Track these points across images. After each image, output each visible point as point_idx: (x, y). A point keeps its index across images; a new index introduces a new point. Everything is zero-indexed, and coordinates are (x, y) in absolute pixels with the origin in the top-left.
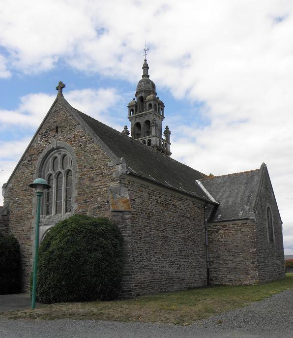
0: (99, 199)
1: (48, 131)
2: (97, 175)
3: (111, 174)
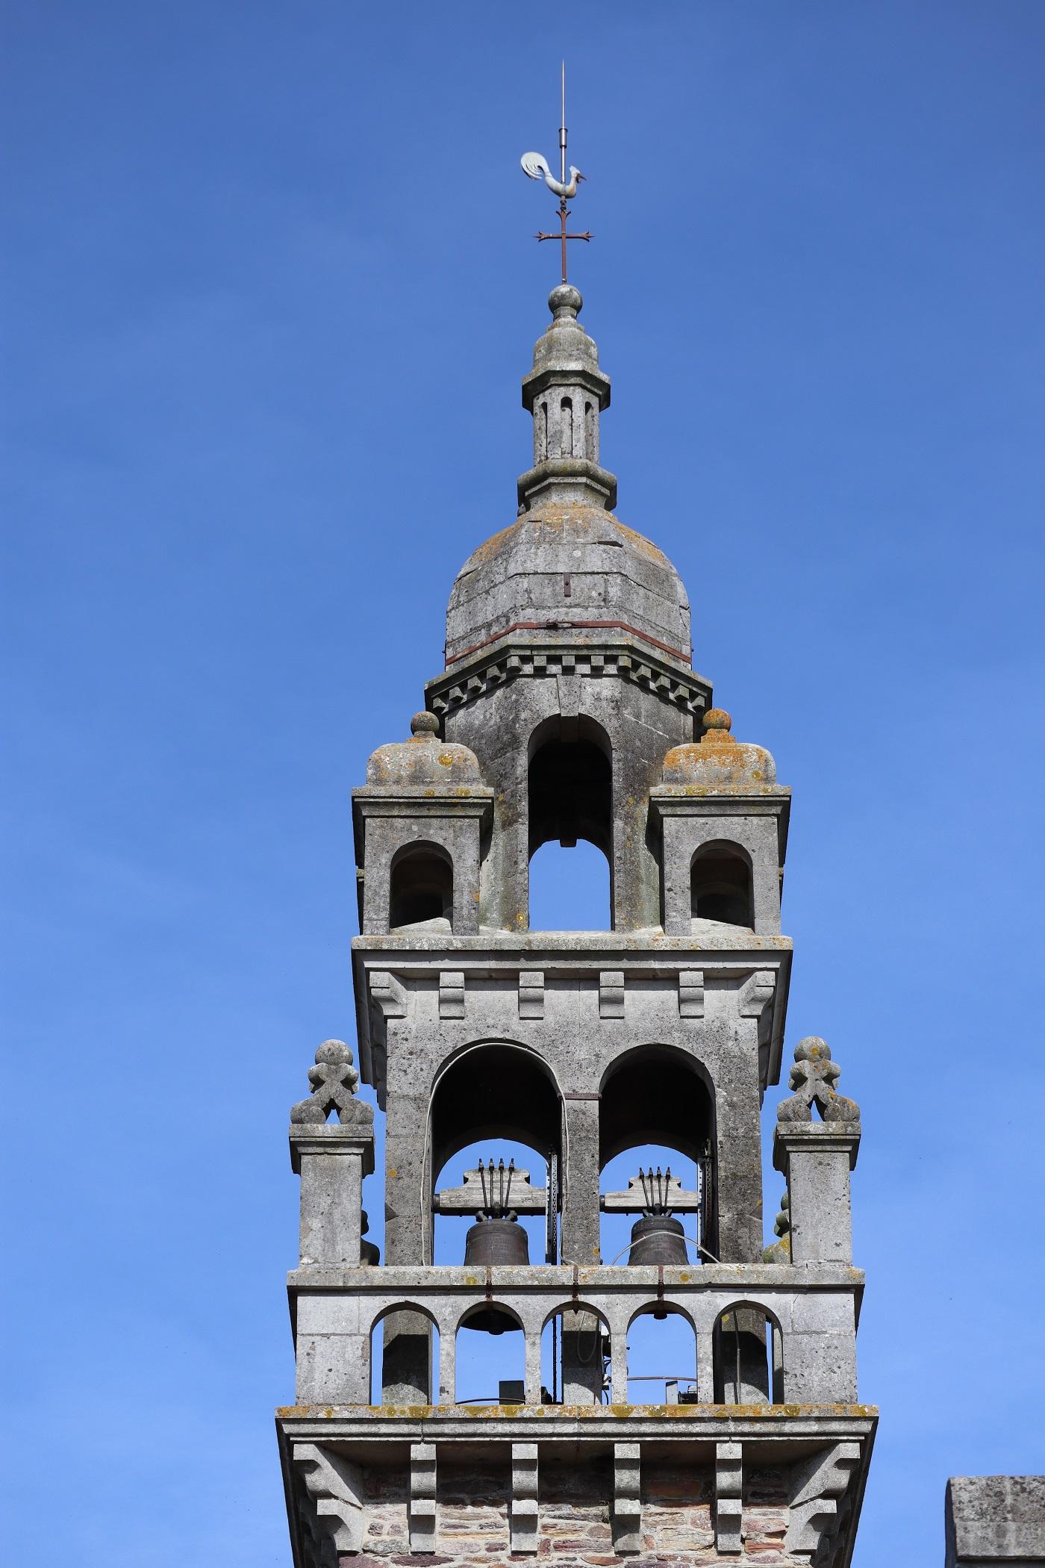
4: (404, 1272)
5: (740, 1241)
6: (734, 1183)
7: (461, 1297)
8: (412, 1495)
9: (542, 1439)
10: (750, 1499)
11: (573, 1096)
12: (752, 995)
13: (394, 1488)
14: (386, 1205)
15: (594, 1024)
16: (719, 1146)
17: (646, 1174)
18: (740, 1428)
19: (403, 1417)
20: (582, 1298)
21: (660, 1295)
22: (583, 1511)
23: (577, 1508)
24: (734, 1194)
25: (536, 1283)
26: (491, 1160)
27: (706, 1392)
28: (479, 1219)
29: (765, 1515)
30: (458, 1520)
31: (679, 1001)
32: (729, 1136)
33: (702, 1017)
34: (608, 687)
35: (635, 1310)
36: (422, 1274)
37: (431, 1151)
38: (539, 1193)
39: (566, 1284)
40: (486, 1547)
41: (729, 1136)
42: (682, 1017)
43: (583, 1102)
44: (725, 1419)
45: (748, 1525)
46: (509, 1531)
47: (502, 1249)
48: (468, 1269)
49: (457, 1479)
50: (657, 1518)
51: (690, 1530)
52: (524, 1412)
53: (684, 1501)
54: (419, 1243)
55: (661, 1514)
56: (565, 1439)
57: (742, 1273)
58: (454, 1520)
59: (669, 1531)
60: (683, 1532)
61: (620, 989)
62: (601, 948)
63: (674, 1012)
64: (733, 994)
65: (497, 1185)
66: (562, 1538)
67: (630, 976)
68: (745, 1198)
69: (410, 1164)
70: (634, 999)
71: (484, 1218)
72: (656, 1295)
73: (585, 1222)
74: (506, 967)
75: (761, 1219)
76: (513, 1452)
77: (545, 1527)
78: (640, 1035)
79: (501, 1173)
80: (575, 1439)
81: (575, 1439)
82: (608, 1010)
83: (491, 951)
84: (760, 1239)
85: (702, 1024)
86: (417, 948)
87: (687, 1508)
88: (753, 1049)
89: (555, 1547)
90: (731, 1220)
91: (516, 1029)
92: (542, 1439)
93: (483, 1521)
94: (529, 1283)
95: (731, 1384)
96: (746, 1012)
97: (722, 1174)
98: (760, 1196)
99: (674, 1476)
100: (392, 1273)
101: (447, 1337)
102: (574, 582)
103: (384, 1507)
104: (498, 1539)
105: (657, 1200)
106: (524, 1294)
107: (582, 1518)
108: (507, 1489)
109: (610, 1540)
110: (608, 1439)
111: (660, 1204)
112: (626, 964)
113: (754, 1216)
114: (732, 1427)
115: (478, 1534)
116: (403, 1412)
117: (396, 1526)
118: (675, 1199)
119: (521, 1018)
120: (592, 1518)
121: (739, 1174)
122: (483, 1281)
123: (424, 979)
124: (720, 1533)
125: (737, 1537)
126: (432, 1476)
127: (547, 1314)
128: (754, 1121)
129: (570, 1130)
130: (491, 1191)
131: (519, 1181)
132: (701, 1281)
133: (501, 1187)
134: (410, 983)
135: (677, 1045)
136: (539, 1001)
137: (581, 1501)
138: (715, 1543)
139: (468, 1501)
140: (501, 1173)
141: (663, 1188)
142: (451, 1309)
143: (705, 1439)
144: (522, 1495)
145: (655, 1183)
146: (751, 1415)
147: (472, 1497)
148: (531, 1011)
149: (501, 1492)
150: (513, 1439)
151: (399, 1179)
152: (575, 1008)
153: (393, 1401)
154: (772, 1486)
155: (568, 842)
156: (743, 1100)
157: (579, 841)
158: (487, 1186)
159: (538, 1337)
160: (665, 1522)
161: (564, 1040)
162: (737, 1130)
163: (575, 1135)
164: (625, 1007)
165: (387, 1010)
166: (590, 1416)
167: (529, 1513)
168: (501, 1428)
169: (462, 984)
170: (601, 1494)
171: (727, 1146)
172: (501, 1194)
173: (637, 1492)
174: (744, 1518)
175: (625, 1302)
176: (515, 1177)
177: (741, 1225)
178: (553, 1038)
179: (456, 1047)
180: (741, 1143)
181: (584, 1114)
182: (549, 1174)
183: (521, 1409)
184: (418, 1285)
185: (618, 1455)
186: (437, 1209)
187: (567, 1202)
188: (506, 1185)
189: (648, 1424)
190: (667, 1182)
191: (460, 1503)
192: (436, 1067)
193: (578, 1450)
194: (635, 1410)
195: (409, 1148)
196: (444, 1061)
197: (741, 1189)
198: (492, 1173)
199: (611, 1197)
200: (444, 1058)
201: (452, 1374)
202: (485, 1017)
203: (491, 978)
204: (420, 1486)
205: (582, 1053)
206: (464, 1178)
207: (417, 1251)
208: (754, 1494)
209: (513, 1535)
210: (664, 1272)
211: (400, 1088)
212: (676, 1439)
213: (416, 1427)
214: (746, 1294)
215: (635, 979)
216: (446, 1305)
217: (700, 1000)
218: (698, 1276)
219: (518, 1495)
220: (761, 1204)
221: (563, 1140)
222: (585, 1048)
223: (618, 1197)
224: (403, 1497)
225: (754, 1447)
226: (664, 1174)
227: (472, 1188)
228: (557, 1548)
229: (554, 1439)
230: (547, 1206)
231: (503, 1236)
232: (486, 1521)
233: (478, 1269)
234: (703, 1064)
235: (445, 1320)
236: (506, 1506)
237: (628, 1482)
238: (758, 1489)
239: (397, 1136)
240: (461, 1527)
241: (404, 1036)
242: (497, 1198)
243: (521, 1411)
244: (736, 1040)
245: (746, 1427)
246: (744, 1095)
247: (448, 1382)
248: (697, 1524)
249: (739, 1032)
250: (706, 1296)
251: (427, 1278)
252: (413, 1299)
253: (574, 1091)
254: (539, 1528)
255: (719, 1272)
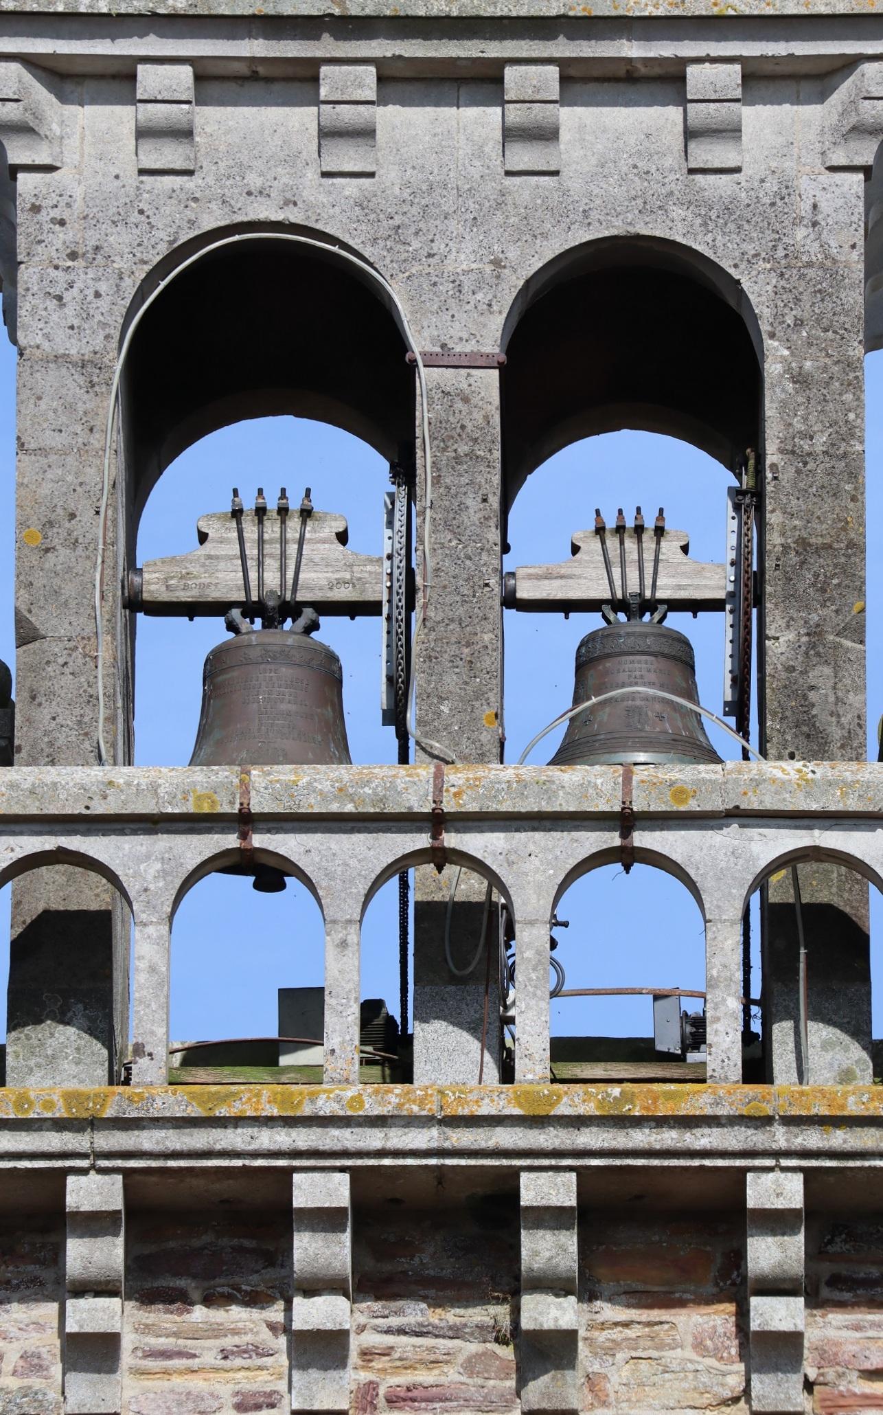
4: (55, 784)
5: (812, 695)
6: (803, 563)
7: (183, 837)
8: (68, 1286)
9: (359, 1162)
10: (825, 1292)
11: (443, 359)
12: (853, 120)
13: (31, 1268)
14: (17, 612)
15: (490, 189)
16: (769, 475)
17: (611, 523)
18: (799, 1140)
19: (49, 1115)
20: (451, 840)
21: (626, 834)
22: (452, 1316)
23: (439, 1311)
24: (801, 586)
25: (349, 808)
26: (260, 491)
27: (724, 1056)
28: (232, 627)
29: (857, 1328)
30: (172, 1340)
31: (685, 132)
32: (793, 452)
33: (737, 170)
35: (569, 867)
36: (94, 788)
37: (122, 485)
38: (369, 568)
39: (415, 810)
40: (235, 1400)
41: (793, 452)
42: (692, 171)
43: (464, 372)
44: (767, 1121)
45: (820, 1351)
46: (286, 1363)
47: (282, 701)
48: (201, 776)
49: (172, 1244)
50: (617, 1334)
51: (691, 1361)
52: (320, 1102)
53: (677, 1295)
54: (92, 699)
55: (626, 1325)
56: (410, 1162)
57: (808, 786)
58: (162, 1340)
59: (644, 1365)
60: (674, 1366)
61: (552, 106)
62: (505, 12)
63: (672, 160)
64: (811, 113)
65: (273, 549)
66: (404, 1379)
67: (572, 72)
68: (827, 596)
69: (72, 516)
70: (582, 128)
71: (244, 624)
72: (617, 834)
73: (466, 651)
74: (290, 55)
75: (862, 642)
76: (295, 1192)
77: (367, 1355)
78: (594, 215)
79: (283, 522)
80: (433, 1162)
81: (433, 1162)
82: (523, 156)
83: (254, 16)
84: (860, 688)
85: (736, 187)
86: (83, 9)
87: (684, 1311)
88: (853, 246)
89: (389, 1401)
90: (794, 647)
91: (312, 198)
92: (359, 1162)
93: (229, 1342)
94: (335, 808)
95: (788, 1025)
96: (839, 159)
97: (774, 539)
98: (861, 591)
99: (656, 1238)
100: (27, 786)
101: (151, 930)
103: (7, 1311)
104: (261, 1382)
105: (633, 587)
106: (323, 832)
107: (450, 1333)
108: (282, 1266)
109: (511, 1383)
110: (505, 1162)
111: (641, 595)
112: (563, 48)
113: (846, 637)
114: (780, 1137)
115: (217, 1370)
116: (49, 1105)
117: (32, 1355)
118: (674, 581)
119: (325, 175)
120: (472, 1334)
121: (813, 540)
122: (232, 803)
123: (100, 77)
124: (759, 1371)
125: (796, 1380)
126: (114, 1245)
127: (374, 876)
128: (851, 416)
129: (433, 438)
130: (260, 564)
131: (324, 541)
132: (716, 803)
133: (283, 555)
134: (68, 87)
135: (679, 239)
136: (366, 133)
137: (449, 1293)
138: (747, 1392)
139: (196, 1295)
140: (283, 522)
141: (649, 556)
142: (158, 866)
143: (720, 1163)
144: (312, 1288)
145: (630, 544)
146: (824, 1111)
147: (206, 1284)
148: (347, 157)
149: (271, 1273)
150: (297, 1163)
151: (47, 550)
152: (447, 150)
153: (32, 1063)
154: (874, 1263)
156: (825, 368)
158: (252, 551)
159: (353, 929)
160: (634, 1343)
161: (422, 225)
162: (811, 438)
163: (444, 450)
164: (562, 147)
165: (17, 153)
166: (466, 1112)
167: (329, 1326)
168: (268, 1139)
169: (189, 95)
170: (492, 1278)
171: (787, 475)
172: (283, 570)
173: (570, 1280)
174: (812, 1336)
175: (546, 850)
176: (314, 531)
177: (815, 660)
178: (398, 220)
179: (175, 241)
180: (819, 468)
181: (466, 400)
182: (390, 524)
183: (313, 1098)
184: (85, 812)
185: (528, 1197)
186: (135, 604)
187: (425, 607)
188: (292, 549)
189: (595, 1129)
190: (658, 543)
191: (177, 1298)
192: (130, 287)
193: (440, 1183)
194: (565, 1099)
195: (70, 478)
196: (150, 274)
197: (816, 576)
198: (261, 522)
199: (530, 577)
200: (148, 268)
201: (162, 1014)
202: (243, 168)
203: (254, 77)
204: (85, 1268)
205: (463, 257)
206: (199, 531)
207: (86, 719)
208: (835, 1281)
209: (296, 1375)
210: (634, 783)
211: (47, 337)
212: (656, 1162)
213: (79, 1136)
214: (816, 832)
215: (586, 80)
216: (148, 857)
217: (732, 132)
218: (712, 792)
219: (305, 1286)
220: (863, 610)
221: (419, 462)
222: (468, 246)
223: (546, 578)
224: (50, 1287)
225: (832, 1179)
226: (650, 523)
227: (217, 557)
229: (387, 1162)
230: (385, 598)
231: (285, 671)
232: (236, 1340)
233: (224, 774)
234: (738, 282)
235: (146, 890)
236: (280, 1305)
237: (550, 1258)
238: (843, 1269)
239: (42, 451)
240: (180, 1354)
241: (55, 213)
242: (272, 579)
243: (313, 1102)
244: (815, 224)
245: (812, 1139)
246: (828, 355)
247: (152, 1033)
248: (706, 1349)
249: (823, 205)
250: (730, 836)
251: (105, 798)
252: (75, 843)
253: (443, 346)
254: (354, 1357)
255: (757, 783)
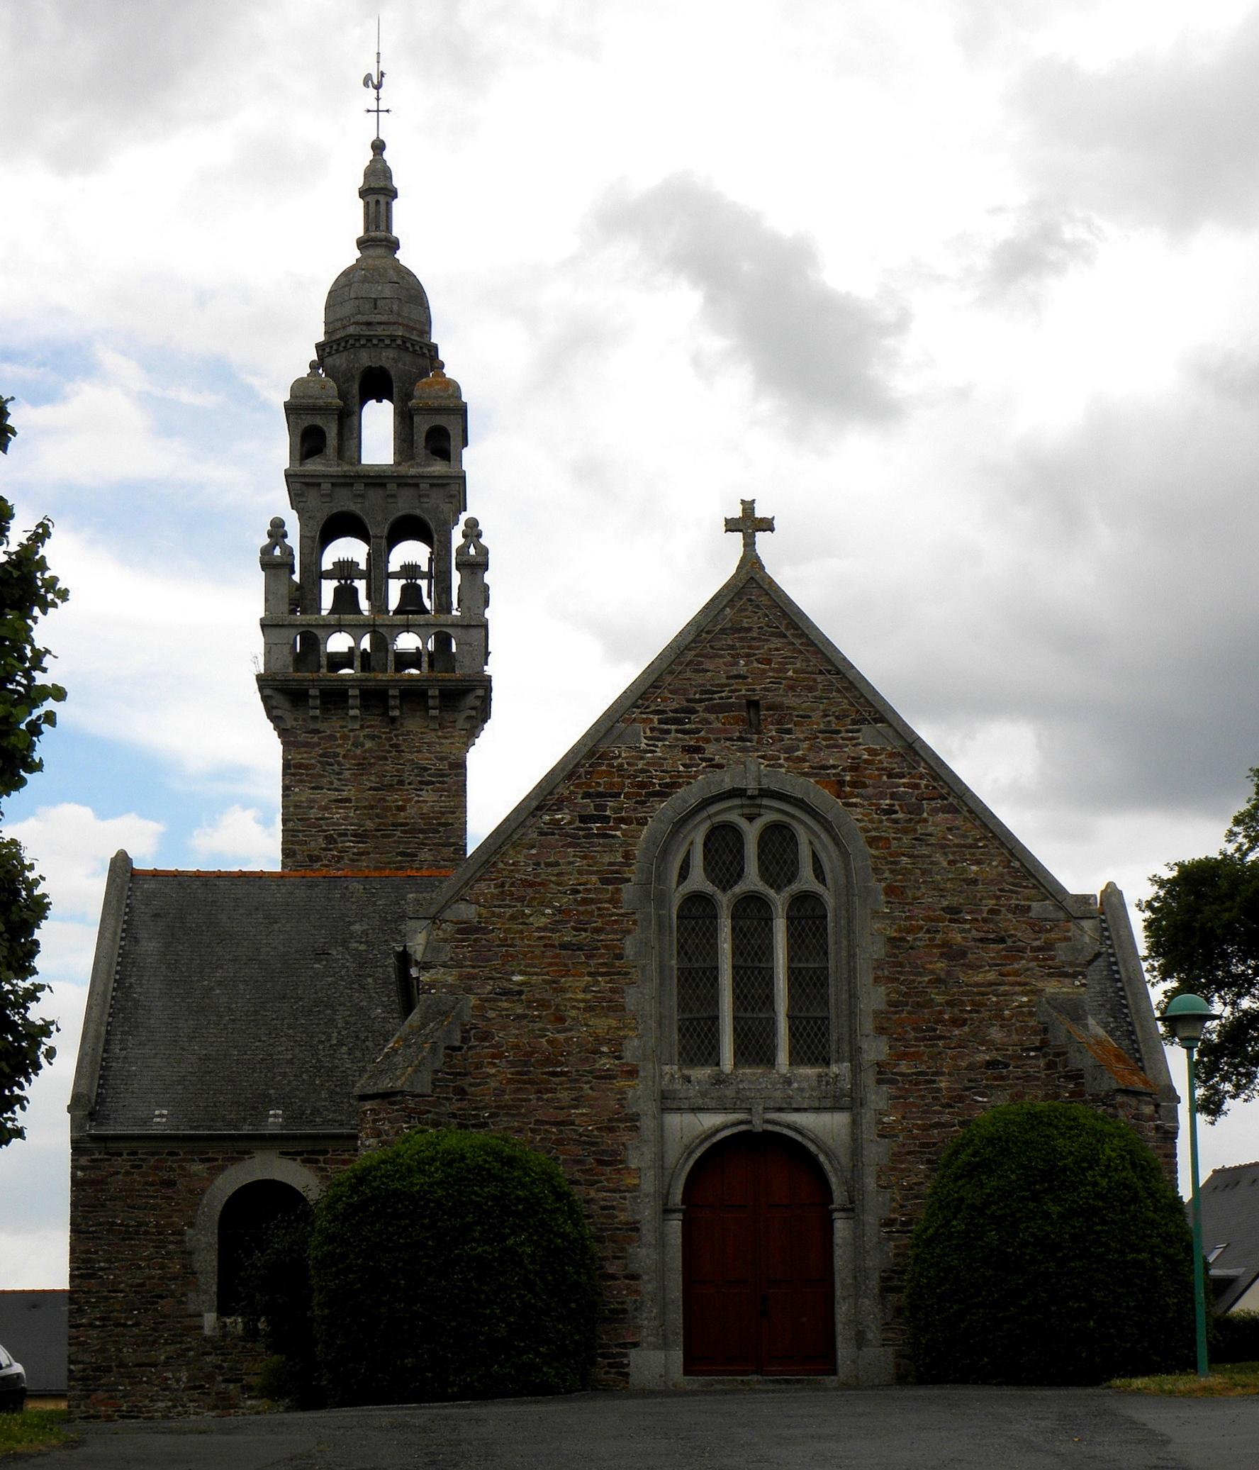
0: (996, 1034)
1: (699, 707)
2: (981, 940)
3: (1048, 946)
34: (391, 353)
96: (446, 500)
102: (379, 302)
114: (434, 683)
155: (379, 401)
157: (331, 567)
228: (368, 727)
